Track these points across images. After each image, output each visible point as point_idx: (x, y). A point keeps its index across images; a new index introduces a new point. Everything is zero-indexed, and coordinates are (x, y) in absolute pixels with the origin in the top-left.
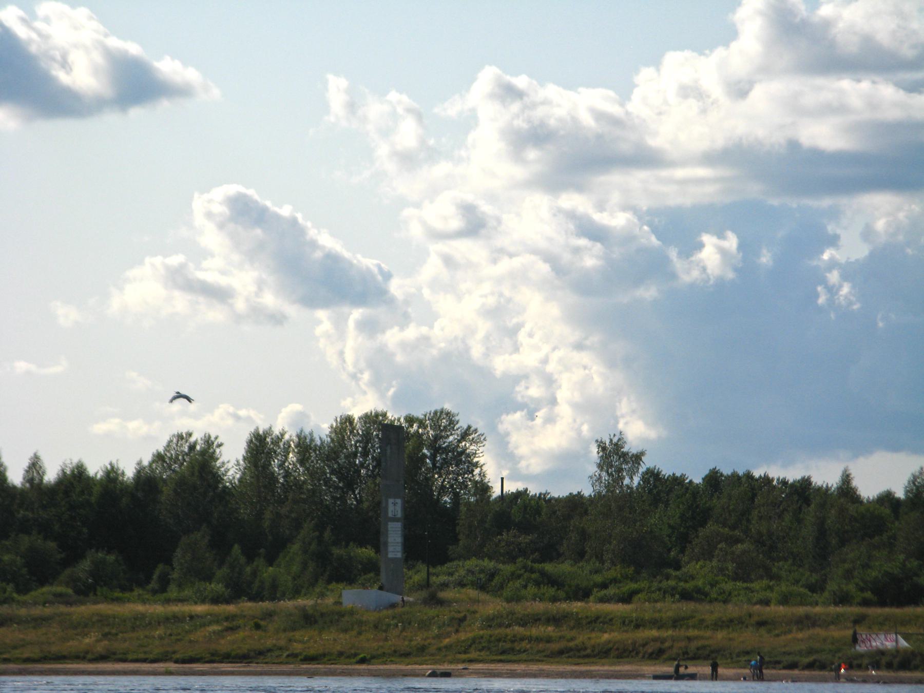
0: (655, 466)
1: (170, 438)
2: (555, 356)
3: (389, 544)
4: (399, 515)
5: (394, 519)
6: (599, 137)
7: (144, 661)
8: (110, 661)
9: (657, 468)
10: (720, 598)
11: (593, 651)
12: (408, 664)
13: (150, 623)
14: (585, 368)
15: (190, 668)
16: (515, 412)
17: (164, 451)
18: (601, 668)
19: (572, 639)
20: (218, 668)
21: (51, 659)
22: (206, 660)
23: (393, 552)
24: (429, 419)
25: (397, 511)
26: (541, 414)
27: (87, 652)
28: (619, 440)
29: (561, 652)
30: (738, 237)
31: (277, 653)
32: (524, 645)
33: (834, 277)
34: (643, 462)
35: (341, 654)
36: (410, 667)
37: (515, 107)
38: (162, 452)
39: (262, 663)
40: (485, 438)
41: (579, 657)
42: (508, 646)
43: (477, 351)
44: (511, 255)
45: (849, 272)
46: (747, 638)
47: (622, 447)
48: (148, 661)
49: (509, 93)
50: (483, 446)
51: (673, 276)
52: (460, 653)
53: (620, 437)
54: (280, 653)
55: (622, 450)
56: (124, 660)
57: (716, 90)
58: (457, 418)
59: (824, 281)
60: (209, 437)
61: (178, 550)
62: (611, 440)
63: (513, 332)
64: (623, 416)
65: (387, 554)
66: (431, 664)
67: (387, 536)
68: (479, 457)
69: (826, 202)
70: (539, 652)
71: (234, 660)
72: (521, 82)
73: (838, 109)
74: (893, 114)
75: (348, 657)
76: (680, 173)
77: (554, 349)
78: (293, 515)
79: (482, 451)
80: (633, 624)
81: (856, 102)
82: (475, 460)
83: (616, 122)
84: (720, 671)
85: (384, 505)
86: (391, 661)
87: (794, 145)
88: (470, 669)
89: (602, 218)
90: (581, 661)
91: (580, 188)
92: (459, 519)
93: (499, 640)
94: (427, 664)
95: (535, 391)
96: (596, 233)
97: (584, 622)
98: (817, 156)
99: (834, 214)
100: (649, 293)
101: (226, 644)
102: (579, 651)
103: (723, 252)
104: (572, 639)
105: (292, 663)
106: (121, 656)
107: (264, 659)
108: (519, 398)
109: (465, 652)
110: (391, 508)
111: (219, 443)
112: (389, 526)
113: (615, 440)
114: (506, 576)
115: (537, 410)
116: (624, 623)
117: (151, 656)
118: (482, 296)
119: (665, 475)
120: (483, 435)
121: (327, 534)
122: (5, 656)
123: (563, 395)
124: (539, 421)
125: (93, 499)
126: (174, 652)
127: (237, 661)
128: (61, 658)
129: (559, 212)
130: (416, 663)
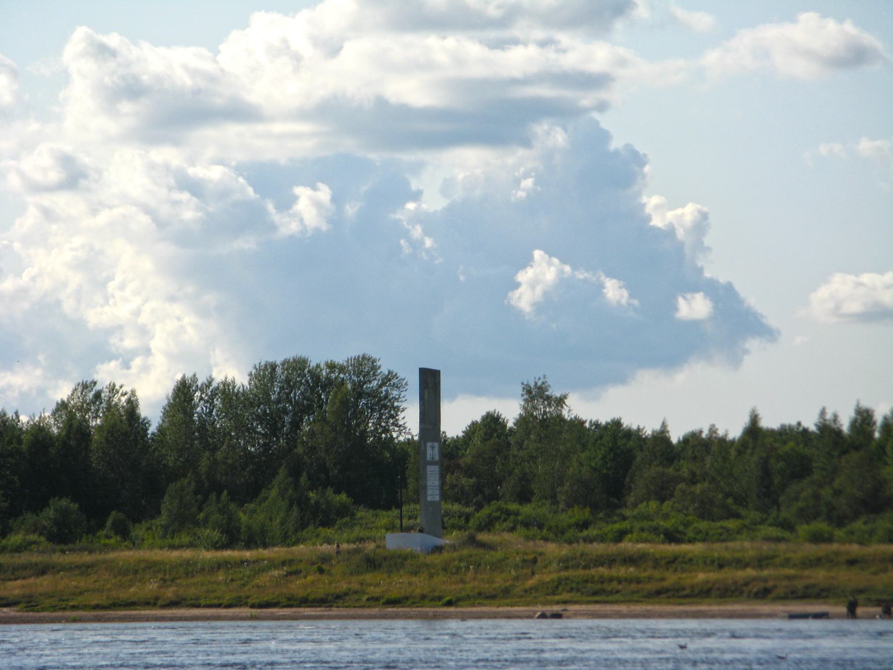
0: (495, 410)
1: (76, 387)
2: (148, 307)
3: (428, 488)
4: (437, 458)
5: (433, 463)
6: (197, 92)
7: (219, 606)
8: (183, 607)
9: (497, 412)
10: (699, 537)
11: (692, 591)
12: (499, 606)
13: (203, 569)
14: (179, 319)
15: (272, 613)
16: (110, 361)
17: (68, 400)
18: (89, 613)
19: (663, 579)
20: (299, 612)
21: (120, 606)
22: (284, 604)
23: (431, 495)
24: (351, 366)
25: (435, 455)
26: (137, 362)
27: (157, 598)
28: (543, 383)
29: (658, 593)
30: (330, 188)
31: (356, 597)
32: (614, 585)
33: (417, 232)
34: (566, 405)
35: (423, 597)
36: (501, 609)
37: (111, 65)
38: (66, 400)
39: (342, 607)
40: (407, 383)
41: (679, 597)
42: (598, 587)
43: (68, 306)
44: (111, 208)
45: (428, 222)
46: (846, 577)
47: (547, 391)
48: (222, 606)
49: (103, 52)
50: (406, 391)
51: (273, 227)
52: (548, 594)
53: (544, 380)
54: (360, 597)
55: (546, 393)
56: (198, 606)
57: (303, 46)
58: (378, 363)
59: (406, 234)
60: (114, 385)
61: (166, 496)
62: (536, 383)
63: (103, 285)
64: (216, 365)
65: (426, 497)
66: (523, 606)
67: (426, 479)
68: (401, 401)
69: (407, 157)
70: (633, 592)
71: (313, 604)
72: (113, 40)
73: (426, 65)
74: (477, 71)
75: (433, 599)
76: (278, 128)
77: (146, 301)
78: (230, 461)
79: (403, 395)
80: (716, 563)
81: (441, 58)
82: (396, 404)
83: (212, 79)
84: (860, 611)
85: (422, 448)
86: (479, 603)
87: (381, 103)
88: (570, 611)
89: (197, 172)
90: (683, 601)
91: (176, 143)
92: (409, 463)
93: (586, 581)
94: (518, 606)
95: (130, 342)
96: (195, 188)
97: (663, 562)
98: (405, 112)
99: (417, 168)
100: (247, 244)
101: (296, 586)
102: (677, 590)
103: (318, 204)
104: (663, 579)
105: (375, 607)
106: (193, 602)
107: (343, 603)
108: (113, 349)
109: (554, 594)
110: (429, 451)
111: (124, 392)
112: (428, 470)
113: (539, 383)
114: (483, 519)
115: (131, 360)
116: (705, 562)
117: (225, 602)
118: (72, 249)
119: (504, 420)
120: (404, 379)
121: (303, 479)
122: (71, 604)
123: (157, 344)
124: (134, 370)
125: (24, 447)
126: (248, 597)
127: (315, 604)
128: (130, 604)
129: (152, 166)
130: (507, 605)
